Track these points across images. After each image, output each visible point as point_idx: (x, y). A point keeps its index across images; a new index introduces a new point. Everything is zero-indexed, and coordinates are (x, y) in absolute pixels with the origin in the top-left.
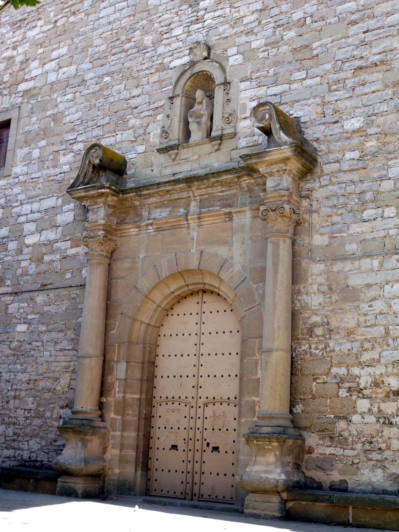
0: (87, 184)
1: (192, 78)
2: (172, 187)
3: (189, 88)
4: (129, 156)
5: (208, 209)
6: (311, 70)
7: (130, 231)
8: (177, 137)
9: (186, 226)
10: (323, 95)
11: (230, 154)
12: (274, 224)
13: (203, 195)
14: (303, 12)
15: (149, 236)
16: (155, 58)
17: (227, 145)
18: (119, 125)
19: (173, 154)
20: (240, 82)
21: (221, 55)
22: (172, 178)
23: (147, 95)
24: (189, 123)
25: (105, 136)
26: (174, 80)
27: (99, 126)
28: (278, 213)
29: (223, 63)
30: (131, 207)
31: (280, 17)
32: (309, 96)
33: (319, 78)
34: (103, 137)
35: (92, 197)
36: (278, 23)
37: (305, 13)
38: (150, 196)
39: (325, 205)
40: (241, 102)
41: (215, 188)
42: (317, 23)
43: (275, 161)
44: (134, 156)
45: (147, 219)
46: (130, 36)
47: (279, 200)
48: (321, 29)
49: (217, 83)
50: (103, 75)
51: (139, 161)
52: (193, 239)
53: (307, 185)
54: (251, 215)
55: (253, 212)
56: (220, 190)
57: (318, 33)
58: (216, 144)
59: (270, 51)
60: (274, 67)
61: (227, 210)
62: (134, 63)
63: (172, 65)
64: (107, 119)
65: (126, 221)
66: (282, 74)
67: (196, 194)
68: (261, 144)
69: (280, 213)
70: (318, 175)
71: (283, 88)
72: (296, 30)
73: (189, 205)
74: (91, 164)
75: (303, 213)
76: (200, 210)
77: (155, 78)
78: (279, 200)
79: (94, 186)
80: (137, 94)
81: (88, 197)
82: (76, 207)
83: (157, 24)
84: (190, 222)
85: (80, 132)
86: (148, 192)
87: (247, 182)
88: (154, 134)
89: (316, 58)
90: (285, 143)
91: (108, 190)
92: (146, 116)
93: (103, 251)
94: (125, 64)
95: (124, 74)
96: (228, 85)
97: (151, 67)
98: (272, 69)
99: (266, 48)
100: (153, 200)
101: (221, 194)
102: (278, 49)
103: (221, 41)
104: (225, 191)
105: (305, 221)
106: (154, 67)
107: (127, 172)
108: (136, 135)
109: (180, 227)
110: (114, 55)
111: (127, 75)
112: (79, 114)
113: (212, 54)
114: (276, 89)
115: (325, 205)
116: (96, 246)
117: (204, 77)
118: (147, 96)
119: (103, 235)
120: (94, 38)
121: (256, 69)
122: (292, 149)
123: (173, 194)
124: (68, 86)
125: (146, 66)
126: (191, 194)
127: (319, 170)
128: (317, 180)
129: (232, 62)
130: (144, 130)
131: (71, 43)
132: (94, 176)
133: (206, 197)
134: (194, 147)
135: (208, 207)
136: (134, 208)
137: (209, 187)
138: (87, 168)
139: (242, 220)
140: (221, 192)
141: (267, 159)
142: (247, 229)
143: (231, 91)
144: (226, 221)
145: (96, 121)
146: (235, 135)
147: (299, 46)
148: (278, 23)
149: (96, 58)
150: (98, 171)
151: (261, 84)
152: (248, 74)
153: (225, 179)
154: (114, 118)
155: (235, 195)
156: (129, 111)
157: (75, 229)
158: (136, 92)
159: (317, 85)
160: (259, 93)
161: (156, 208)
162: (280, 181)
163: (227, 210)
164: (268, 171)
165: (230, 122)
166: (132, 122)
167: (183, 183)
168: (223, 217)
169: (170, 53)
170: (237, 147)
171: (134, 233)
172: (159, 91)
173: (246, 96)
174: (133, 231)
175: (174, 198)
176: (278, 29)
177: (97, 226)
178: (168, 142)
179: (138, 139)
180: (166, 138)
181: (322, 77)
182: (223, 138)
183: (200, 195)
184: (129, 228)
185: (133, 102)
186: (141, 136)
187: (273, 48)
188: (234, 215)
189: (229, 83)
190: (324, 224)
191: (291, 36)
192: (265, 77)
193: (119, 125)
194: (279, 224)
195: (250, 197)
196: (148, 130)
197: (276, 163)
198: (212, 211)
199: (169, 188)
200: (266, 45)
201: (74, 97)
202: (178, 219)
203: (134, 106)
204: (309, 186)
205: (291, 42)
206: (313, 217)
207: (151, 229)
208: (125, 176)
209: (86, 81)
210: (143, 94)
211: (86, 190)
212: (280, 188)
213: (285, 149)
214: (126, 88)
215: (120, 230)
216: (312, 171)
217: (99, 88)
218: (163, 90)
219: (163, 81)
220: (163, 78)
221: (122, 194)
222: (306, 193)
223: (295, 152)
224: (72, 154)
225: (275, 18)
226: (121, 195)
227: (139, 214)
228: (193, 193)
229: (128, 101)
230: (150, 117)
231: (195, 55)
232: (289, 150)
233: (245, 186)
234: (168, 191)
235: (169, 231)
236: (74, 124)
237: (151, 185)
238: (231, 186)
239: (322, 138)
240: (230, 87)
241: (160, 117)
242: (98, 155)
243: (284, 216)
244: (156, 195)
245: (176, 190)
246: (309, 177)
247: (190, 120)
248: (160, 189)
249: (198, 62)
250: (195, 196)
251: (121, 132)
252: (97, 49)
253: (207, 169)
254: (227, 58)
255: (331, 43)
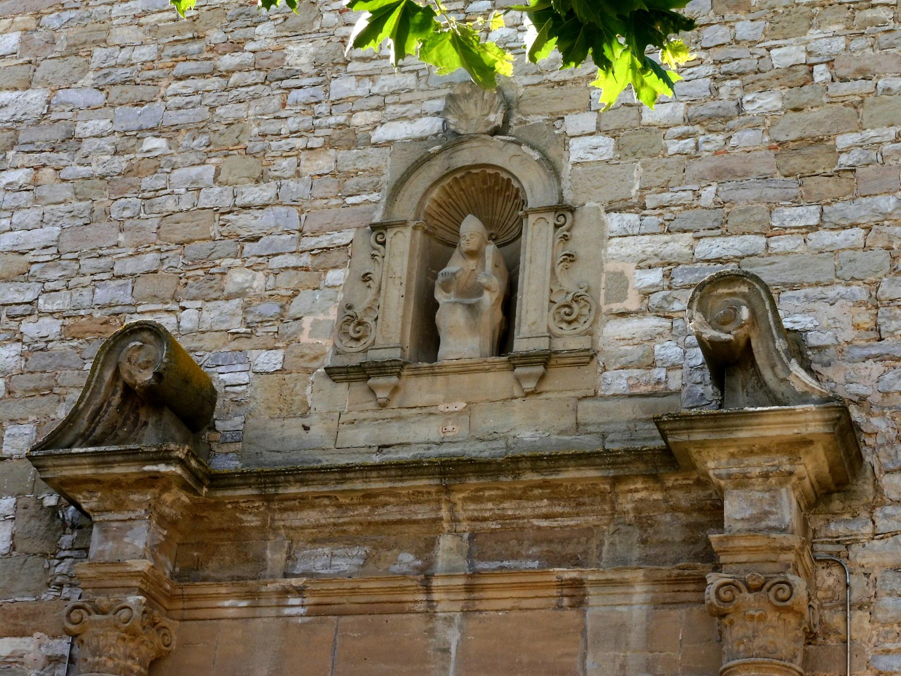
0: (95, 443)
1: (449, 180)
2: (388, 485)
3: (434, 207)
4: (227, 377)
5: (499, 564)
6: (834, 205)
7: (220, 604)
8: (396, 340)
9: (421, 607)
10: (873, 279)
11: (576, 411)
12: (755, 631)
13: (485, 519)
14: (803, 48)
15: (287, 626)
16: (323, 108)
17: (563, 383)
18: (190, 281)
19: (384, 387)
20: (607, 212)
21: (545, 128)
22: (376, 459)
23: (295, 209)
24: (436, 306)
25: (140, 309)
26: (388, 178)
27: (119, 277)
28: (772, 598)
29: (552, 153)
30: (228, 530)
31: (734, 52)
32: (831, 277)
33: (859, 233)
34: (132, 309)
35: (116, 484)
36: (724, 68)
37: (809, 53)
38: (305, 502)
39: (892, 590)
40: (610, 267)
41: (530, 504)
42: (845, 85)
43: (765, 443)
44: (244, 378)
45: (278, 571)
46: (239, 34)
47: (767, 561)
48: (862, 102)
49: (531, 204)
50: (141, 130)
51: (261, 397)
52: (446, 651)
53: (832, 526)
54: (649, 596)
55: (658, 588)
56: (544, 510)
57: (852, 109)
58: (528, 377)
59: (701, 139)
60: (715, 185)
61: (569, 574)
62: (251, 112)
63: (380, 134)
64: (149, 260)
65: (202, 574)
66: (742, 205)
67: (461, 514)
68: (678, 392)
69: (776, 597)
70: (865, 500)
71: (746, 244)
72: (784, 92)
73: (431, 544)
74: (120, 384)
75: (821, 607)
76: (471, 565)
77: (324, 163)
78: (767, 561)
79: (135, 452)
80: (259, 202)
81: (98, 482)
82: (22, 511)
83: (332, 15)
84: (436, 596)
85: (49, 286)
86: (304, 490)
87: (638, 496)
88: (315, 324)
89: (850, 175)
90: (804, 397)
91: (177, 470)
92: (287, 268)
93: (133, 658)
94: (220, 111)
95: (215, 138)
96: (569, 215)
97: (312, 130)
98: (712, 189)
99: (690, 129)
100: (310, 516)
101: (545, 523)
102: (728, 135)
103: (544, 91)
104: (562, 515)
105: (827, 631)
106: (318, 132)
107: (217, 422)
108: (250, 318)
109: (400, 608)
110: (180, 79)
111: (219, 142)
112: (50, 233)
113: (513, 121)
114: (725, 245)
115: (892, 590)
116: (112, 640)
117: (485, 183)
118: (294, 212)
119: (143, 608)
120: (115, 22)
121: (659, 182)
122: (827, 416)
123: (385, 505)
124: (13, 144)
125: (292, 124)
126: (444, 513)
127: (869, 488)
128: (864, 515)
129: (581, 154)
130: (282, 307)
131: (32, 24)
132: (120, 421)
133: (493, 525)
134: (452, 377)
135: (500, 557)
136: (239, 534)
137: (511, 497)
138: (106, 395)
139: (619, 608)
140: (546, 517)
141: (743, 434)
142: (635, 637)
143: (576, 232)
144: (561, 607)
145: (109, 259)
146: (592, 357)
147: (793, 136)
148: (724, 68)
149: (118, 80)
150: (137, 408)
151: (674, 225)
152: (633, 192)
153: (567, 480)
154: (176, 261)
155: (589, 531)
156: (229, 246)
157: (13, 580)
158: (253, 194)
159: (855, 249)
160: (668, 249)
161: (314, 541)
162: (770, 505)
163: (569, 574)
164: (734, 470)
165: (576, 320)
166: (238, 278)
167: (430, 475)
168: (554, 592)
169: (374, 102)
170: (596, 393)
171: (231, 613)
172: (334, 202)
173: (625, 251)
174: (231, 605)
175: (385, 518)
176: (728, 83)
177: (120, 575)
178: (365, 351)
179: (260, 331)
180: (358, 340)
181: (869, 229)
182: (553, 362)
183: (476, 519)
184: (218, 597)
185: (245, 222)
186: (270, 322)
187: (710, 131)
188: (591, 591)
189: (572, 210)
190: (888, 646)
191: (769, 106)
192: (686, 207)
193: (190, 281)
194: (771, 630)
195: (644, 542)
196: (294, 309)
197: (765, 450)
198: (511, 572)
199: (376, 485)
200: (689, 120)
201: (35, 179)
202: (397, 584)
203: (245, 234)
204: (837, 528)
205: (768, 122)
206: (855, 621)
207: (295, 606)
208: (207, 435)
209: (80, 140)
210: (281, 204)
211: (100, 460)
212: (772, 524)
213: (805, 412)
214: (221, 178)
215: (182, 597)
216: (848, 487)
217: (125, 165)
218: (350, 200)
219: (348, 175)
220: (351, 169)
221: (209, 487)
222: (830, 548)
223: (834, 425)
224: (17, 347)
225: (719, 54)
226: (205, 490)
227: (251, 555)
228: (451, 510)
229: (227, 217)
230: (302, 274)
231: (464, 117)
232: (818, 417)
233: (629, 506)
234: (368, 496)
235: (361, 617)
236: (29, 257)
237: (318, 471)
238: (584, 504)
239: (876, 398)
240: (574, 221)
241: (335, 276)
242: (151, 358)
243: (789, 610)
244: (326, 502)
245: (396, 495)
246: (836, 505)
247: (440, 296)
248: (346, 487)
249: (471, 138)
250: (455, 520)
251: (199, 304)
252: (123, 55)
253: (494, 445)
254: (564, 140)
255: (892, 142)
